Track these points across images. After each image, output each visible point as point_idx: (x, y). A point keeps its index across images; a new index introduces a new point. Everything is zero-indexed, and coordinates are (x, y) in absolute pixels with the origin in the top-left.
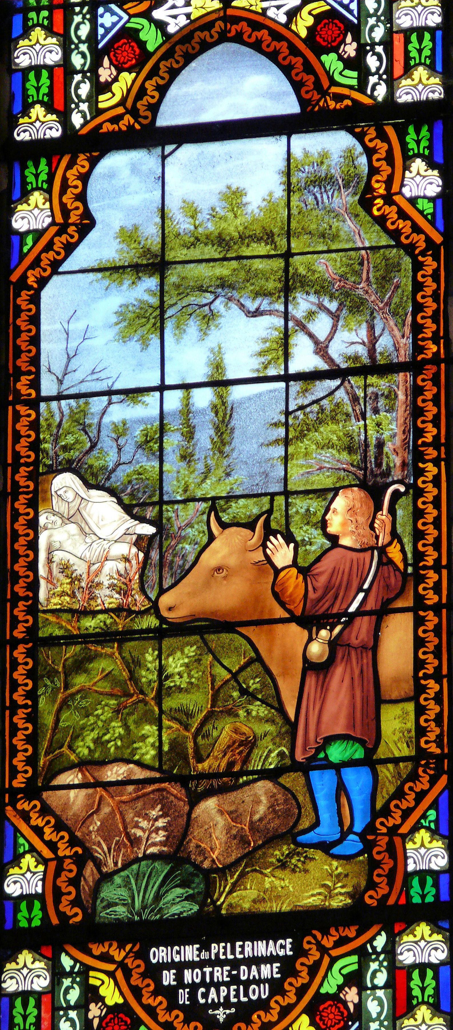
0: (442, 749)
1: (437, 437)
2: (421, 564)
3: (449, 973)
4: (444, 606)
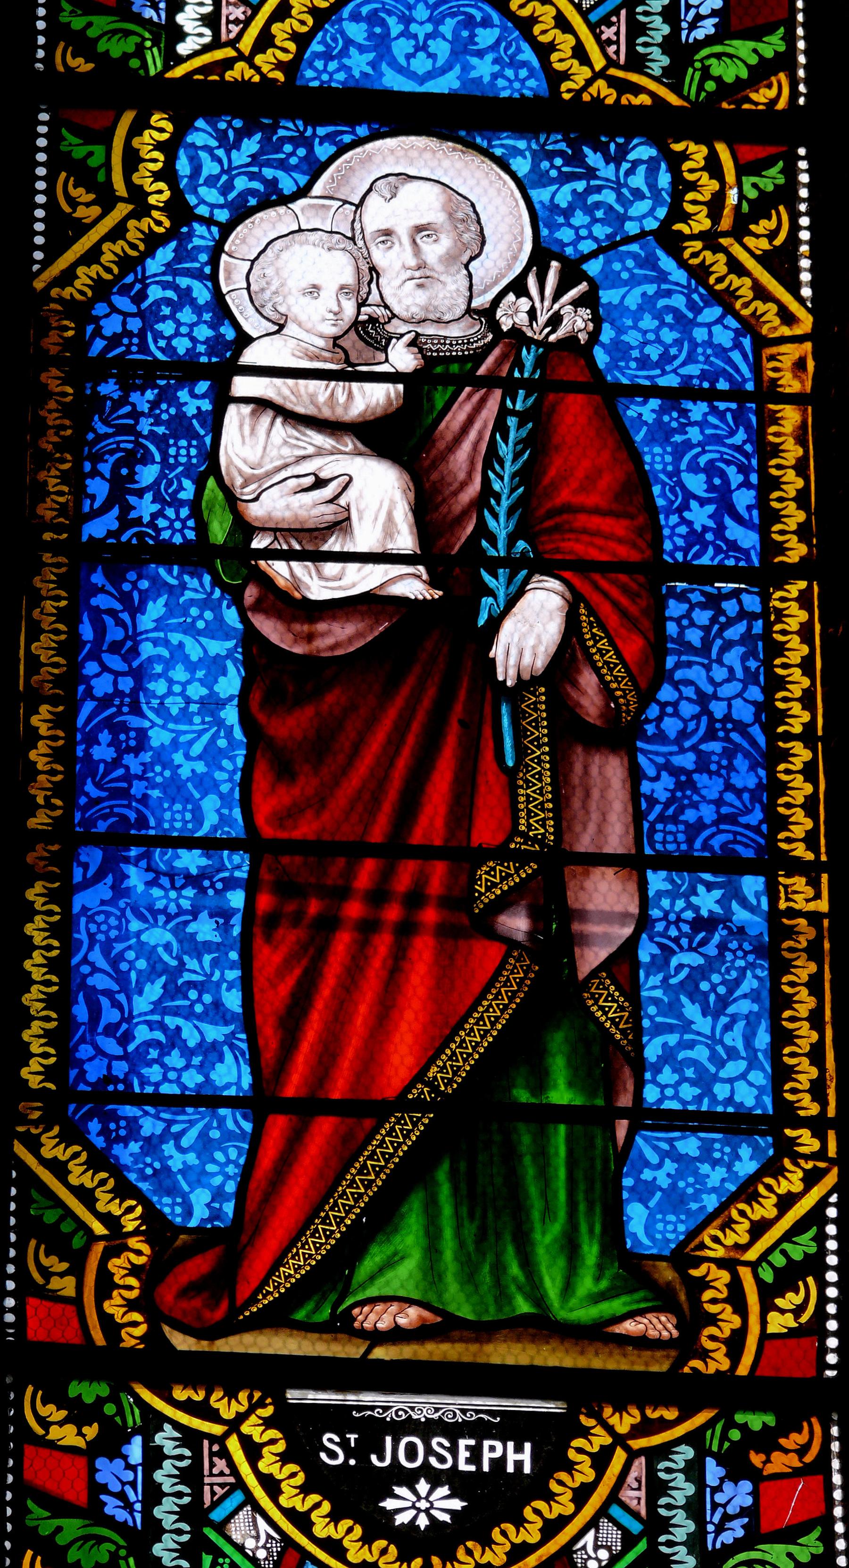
0: (817, 854)
1: (809, 727)
2: (780, 729)
3: (798, 1374)
4: (831, 1124)
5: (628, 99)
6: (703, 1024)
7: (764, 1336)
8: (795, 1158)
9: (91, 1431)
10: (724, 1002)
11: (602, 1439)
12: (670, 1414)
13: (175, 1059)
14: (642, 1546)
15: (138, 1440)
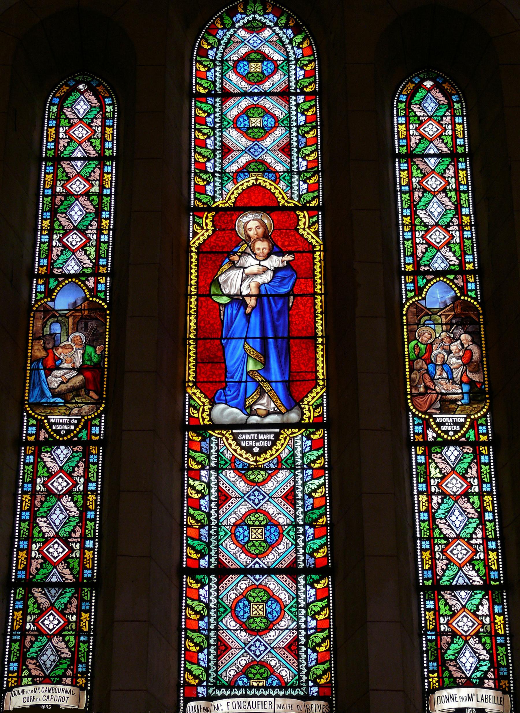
5: (289, 205)
6: (301, 244)
7: (314, 417)
8: (319, 385)
9: (198, 648)
10: (306, 304)
11: (285, 435)
12: (297, 430)
13: (214, 377)
14: (295, 600)
15: (206, 650)
